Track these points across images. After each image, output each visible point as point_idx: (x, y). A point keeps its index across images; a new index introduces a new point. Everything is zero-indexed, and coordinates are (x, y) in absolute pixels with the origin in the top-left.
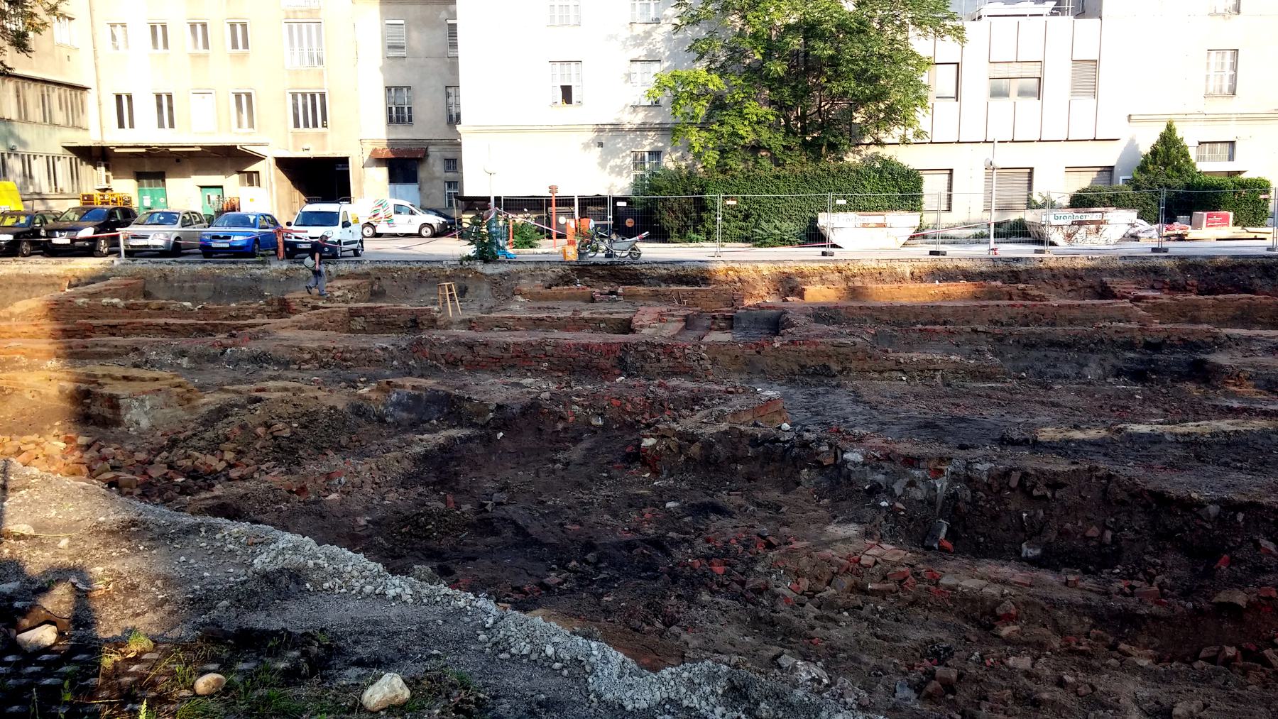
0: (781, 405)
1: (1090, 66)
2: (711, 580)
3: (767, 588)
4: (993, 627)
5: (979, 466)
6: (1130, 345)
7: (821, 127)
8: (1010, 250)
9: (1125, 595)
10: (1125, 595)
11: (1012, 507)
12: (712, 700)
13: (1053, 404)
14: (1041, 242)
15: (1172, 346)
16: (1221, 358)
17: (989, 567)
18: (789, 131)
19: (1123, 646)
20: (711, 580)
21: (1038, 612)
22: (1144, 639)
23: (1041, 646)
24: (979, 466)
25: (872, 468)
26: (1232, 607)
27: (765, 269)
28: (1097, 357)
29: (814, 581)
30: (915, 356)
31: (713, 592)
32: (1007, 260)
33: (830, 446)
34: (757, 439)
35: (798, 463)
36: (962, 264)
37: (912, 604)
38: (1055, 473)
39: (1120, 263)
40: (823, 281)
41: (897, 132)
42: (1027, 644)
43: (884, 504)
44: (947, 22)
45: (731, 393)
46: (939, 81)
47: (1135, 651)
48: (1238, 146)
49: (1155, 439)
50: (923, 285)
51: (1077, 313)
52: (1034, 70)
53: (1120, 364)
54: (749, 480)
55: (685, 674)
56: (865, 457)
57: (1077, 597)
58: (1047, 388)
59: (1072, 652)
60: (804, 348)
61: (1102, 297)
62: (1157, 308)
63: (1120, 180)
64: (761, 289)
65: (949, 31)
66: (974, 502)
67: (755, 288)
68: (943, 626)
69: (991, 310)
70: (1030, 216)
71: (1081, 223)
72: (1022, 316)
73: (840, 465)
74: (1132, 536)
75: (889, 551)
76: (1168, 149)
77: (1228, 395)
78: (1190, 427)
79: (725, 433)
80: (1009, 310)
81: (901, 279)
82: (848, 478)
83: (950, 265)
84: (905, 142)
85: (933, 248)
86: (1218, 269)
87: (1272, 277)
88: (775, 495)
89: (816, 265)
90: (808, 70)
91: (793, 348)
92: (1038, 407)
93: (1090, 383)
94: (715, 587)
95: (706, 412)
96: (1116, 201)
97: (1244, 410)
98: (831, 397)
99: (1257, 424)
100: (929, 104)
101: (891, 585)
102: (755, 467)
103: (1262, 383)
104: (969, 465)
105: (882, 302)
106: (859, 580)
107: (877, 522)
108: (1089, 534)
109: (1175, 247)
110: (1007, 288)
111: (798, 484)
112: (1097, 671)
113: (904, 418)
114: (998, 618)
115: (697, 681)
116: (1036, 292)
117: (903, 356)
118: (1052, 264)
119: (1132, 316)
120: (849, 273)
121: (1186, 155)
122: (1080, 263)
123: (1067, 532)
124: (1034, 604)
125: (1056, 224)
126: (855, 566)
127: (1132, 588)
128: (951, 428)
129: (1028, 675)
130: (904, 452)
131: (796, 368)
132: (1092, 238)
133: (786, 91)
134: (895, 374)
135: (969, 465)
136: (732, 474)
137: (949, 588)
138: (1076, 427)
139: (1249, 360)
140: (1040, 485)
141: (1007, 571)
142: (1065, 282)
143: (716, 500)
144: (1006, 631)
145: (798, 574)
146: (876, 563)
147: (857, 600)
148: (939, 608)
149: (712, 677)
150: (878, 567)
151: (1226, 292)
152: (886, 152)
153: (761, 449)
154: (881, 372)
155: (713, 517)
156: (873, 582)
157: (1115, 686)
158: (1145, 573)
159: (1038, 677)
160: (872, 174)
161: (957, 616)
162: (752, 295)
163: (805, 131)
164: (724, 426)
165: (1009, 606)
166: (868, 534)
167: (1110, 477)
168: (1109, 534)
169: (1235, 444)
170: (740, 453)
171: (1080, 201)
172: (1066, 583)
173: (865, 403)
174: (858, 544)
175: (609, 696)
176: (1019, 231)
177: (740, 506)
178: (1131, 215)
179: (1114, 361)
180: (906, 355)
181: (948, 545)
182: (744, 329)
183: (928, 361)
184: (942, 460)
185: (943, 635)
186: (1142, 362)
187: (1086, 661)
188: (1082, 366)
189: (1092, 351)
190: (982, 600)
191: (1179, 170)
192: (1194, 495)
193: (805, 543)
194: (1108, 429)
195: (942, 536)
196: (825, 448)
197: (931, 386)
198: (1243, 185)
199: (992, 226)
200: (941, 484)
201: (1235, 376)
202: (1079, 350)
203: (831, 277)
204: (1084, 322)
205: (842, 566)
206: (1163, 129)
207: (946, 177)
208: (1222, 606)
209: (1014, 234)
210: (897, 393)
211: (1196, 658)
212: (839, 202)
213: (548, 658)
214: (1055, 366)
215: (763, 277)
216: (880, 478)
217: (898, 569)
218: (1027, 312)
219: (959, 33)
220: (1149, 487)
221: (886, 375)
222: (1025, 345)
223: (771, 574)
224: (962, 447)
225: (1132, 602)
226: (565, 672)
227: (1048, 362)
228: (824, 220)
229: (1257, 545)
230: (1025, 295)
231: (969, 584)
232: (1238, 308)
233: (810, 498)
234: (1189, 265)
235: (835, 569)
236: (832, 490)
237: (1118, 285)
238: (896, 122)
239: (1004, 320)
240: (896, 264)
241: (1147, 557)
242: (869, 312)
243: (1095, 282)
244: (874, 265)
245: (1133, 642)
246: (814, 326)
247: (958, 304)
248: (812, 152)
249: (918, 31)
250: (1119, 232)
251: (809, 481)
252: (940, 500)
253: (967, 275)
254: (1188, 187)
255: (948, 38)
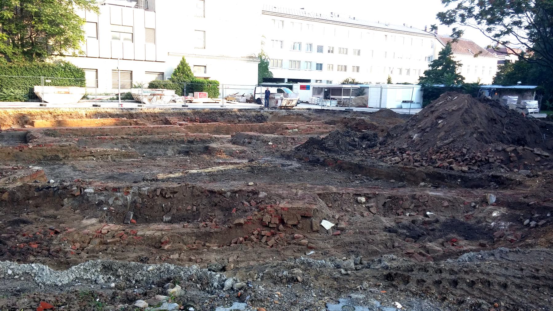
0: (43, 173)
1: (152, 31)
2: (32, 251)
3: (61, 250)
4: (161, 247)
5: (144, 189)
6: (183, 142)
7: (32, 44)
8: (128, 105)
9: (205, 227)
10: (205, 227)
11: (158, 203)
12: (97, 274)
13: (158, 166)
14: (140, 102)
15: (197, 141)
16: (213, 145)
17: (154, 226)
18: (15, 46)
19: (207, 244)
20: (32, 251)
21: (176, 238)
22: (213, 241)
23: (180, 249)
24: (144, 189)
25: (98, 194)
26: (240, 224)
27: (11, 112)
28: (171, 147)
29: (82, 243)
30: (99, 149)
31: (34, 256)
32: (127, 109)
33: (77, 187)
34: (39, 188)
35: (61, 197)
36: (109, 110)
37: (127, 245)
38: (173, 188)
39: (172, 111)
40: (42, 118)
41: (70, 51)
42: (175, 250)
43: (105, 209)
44: (90, 4)
45: (16, 169)
46: (88, 29)
47: (211, 245)
48: (207, 67)
49: (199, 175)
50: (92, 120)
51: (160, 130)
52: (130, 30)
53: (179, 149)
54: (37, 207)
55: (82, 267)
56: (95, 190)
57: (189, 230)
58: (154, 159)
59: (191, 249)
60: (45, 148)
61: (165, 124)
62: (188, 128)
63: (167, 78)
64: (9, 122)
65: (92, 8)
66: (143, 202)
67: (5, 121)
68: (142, 250)
69: (127, 130)
70: (134, 91)
71: (154, 95)
72: (136, 132)
73: (83, 195)
74: (203, 207)
75: (112, 226)
76: (183, 67)
77: (218, 158)
78: (210, 170)
79: (21, 186)
80: (133, 129)
81: (81, 117)
82: (87, 200)
83: (103, 111)
84: (74, 55)
85: (94, 104)
86: (206, 113)
87: (223, 117)
88: (51, 212)
89: (38, 110)
90: (22, 18)
91: (39, 148)
92: (153, 167)
93: (170, 157)
94: (35, 254)
95: (5, 178)
96: (165, 86)
97: (224, 163)
98: (62, 169)
99: (231, 167)
100: (85, 40)
101: (118, 239)
102: (39, 201)
103: (228, 153)
104: (139, 188)
105: (74, 127)
106: (102, 239)
107: (103, 217)
108: (188, 209)
109: (191, 106)
110: (129, 121)
111: (63, 206)
112: (201, 254)
113: (99, 176)
114: (162, 243)
115: (88, 268)
116: (142, 123)
117: (93, 150)
118: (146, 111)
119: (181, 130)
120: (56, 114)
121: (190, 70)
122: (157, 111)
123: (180, 209)
124: (175, 236)
125: (144, 93)
126: (100, 234)
127: (206, 224)
128: (121, 178)
129: (178, 260)
130: (112, 186)
131: (41, 157)
132: (159, 101)
133: (13, 26)
134: (90, 157)
135: (139, 188)
136: (27, 205)
137: (142, 236)
138: (171, 173)
139: (223, 145)
140: (168, 193)
141: (161, 226)
142: (151, 118)
143: (21, 217)
144: (166, 247)
145: (74, 242)
146: (108, 232)
147: (103, 247)
148: (139, 244)
149: (95, 266)
150: (109, 233)
151: (210, 122)
152: (66, 59)
153: (42, 192)
154: (84, 157)
155: (22, 225)
156: (109, 239)
157: (208, 257)
158: (209, 218)
159: (182, 260)
160: (61, 69)
161: (146, 245)
162: (4, 125)
163: (23, 46)
164: (19, 184)
165: (166, 238)
166: (101, 222)
167: (193, 187)
168: (195, 208)
169: (225, 174)
170: (30, 195)
171: (152, 86)
172: (184, 227)
173: (79, 171)
174: (98, 226)
175: (48, 282)
176: (129, 97)
177: (36, 219)
178: (173, 92)
179: (178, 148)
180: (94, 149)
181: (134, 221)
182: (6, 141)
183: (104, 151)
184: (128, 188)
185: (143, 253)
186: (187, 148)
187: (197, 251)
188: (166, 150)
189: (169, 144)
190: (155, 238)
191: (188, 76)
192: (223, 190)
193: (74, 229)
194: (182, 173)
195: (131, 218)
196: (75, 188)
197: (107, 162)
198: (210, 83)
199: (120, 95)
200: (129, 197)
201: (219, 151)
202: (164, 144)
203: (46, 116)
204: (163, 133)
205: (94, 235)
206: (181, 59)
207: (95, 73)
208: (236, 225)
209: (127, 98)
210: (92, 165)
211: (231, 244)
212: (47, 81)
213: (10, 275)
214: (156, 151)
215: (10, 116)
216: (102, 198)
217: (119, 232)
218: (141, 130)
219: (96, 9)
220: (207, 189)
221: (86, 158)
222: (143, 143)
223: (61, 244)
224: (135, 182)
225: (208, 229)
226: (22, 278)
227: (152, 149)
228: (38, 89)
229: (243, 204)
230: (137, 123)
231: (148, 233)
232: (215, 127)
233: (70, 211)
234: (196, 112)
235: (91, 237)
236: (80, 206)
237: (172, 119)
238: (70, 46)
239: (132, 133)
240: (78, 110)
241: (209, 213)
242: (71, 131)
243: (163, 118)
244: (68, 110)
245: (210, 242)
246: (47, 138)
247: (112, 127)
248: (28, 57)
249: (78, 6)
250: (169, 100)
251: (68, 203)
252: (129, 204)
253: (111, 115)
254: (192, 82)
255: (92, 11)
